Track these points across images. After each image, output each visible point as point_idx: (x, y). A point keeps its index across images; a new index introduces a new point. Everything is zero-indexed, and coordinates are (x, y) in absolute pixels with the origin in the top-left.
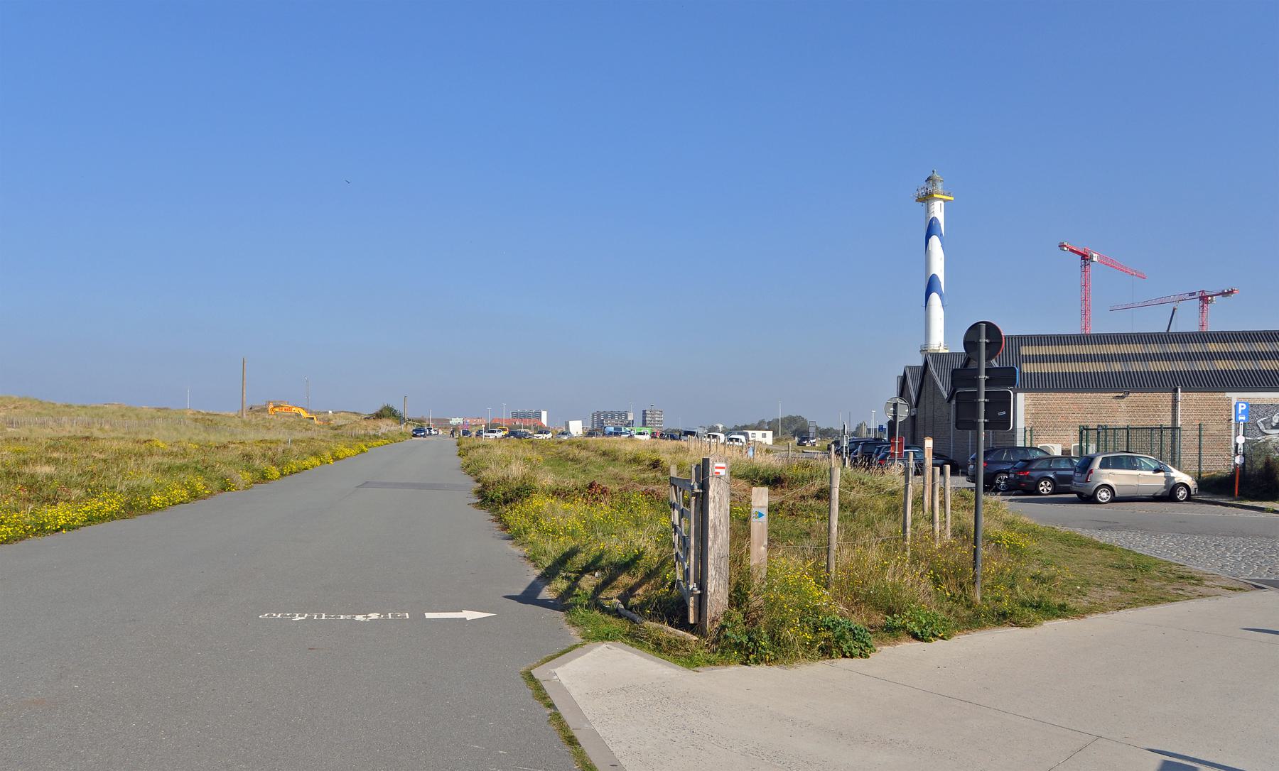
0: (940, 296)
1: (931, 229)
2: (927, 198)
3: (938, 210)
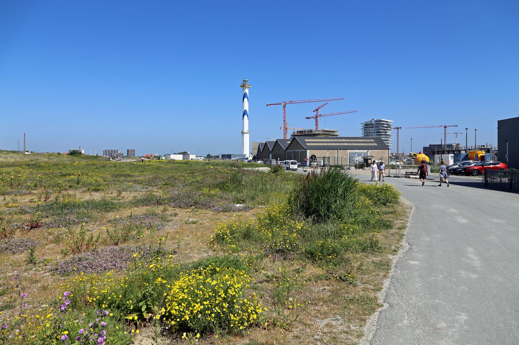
0: (248, 116)
1: (245, 96)
2: (243, 86)
3: (247, 91)
